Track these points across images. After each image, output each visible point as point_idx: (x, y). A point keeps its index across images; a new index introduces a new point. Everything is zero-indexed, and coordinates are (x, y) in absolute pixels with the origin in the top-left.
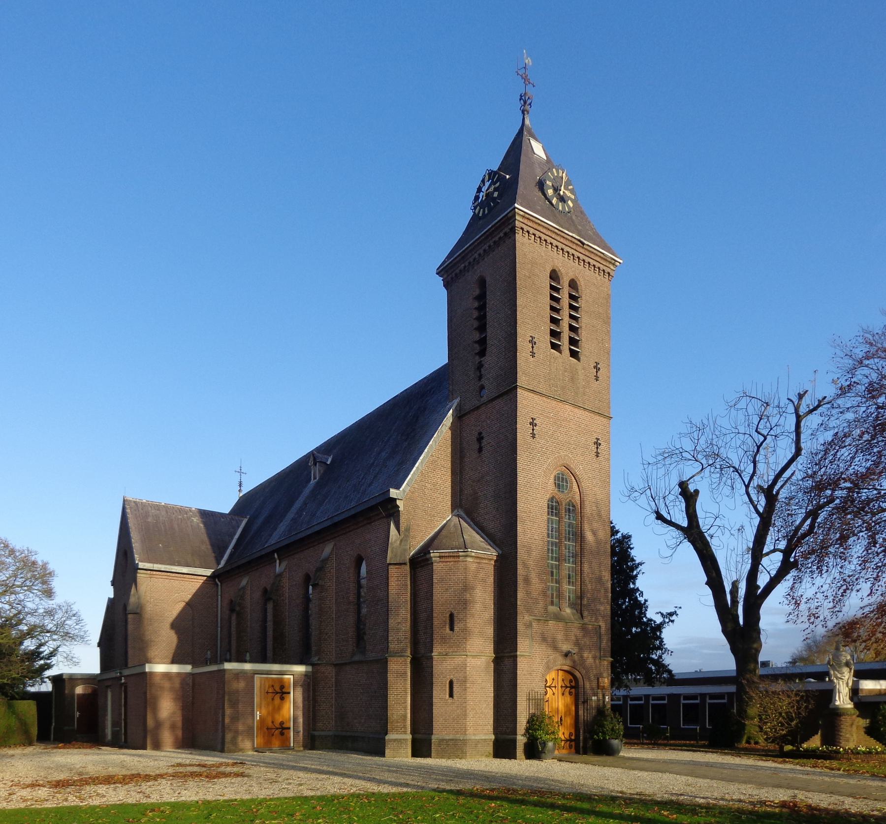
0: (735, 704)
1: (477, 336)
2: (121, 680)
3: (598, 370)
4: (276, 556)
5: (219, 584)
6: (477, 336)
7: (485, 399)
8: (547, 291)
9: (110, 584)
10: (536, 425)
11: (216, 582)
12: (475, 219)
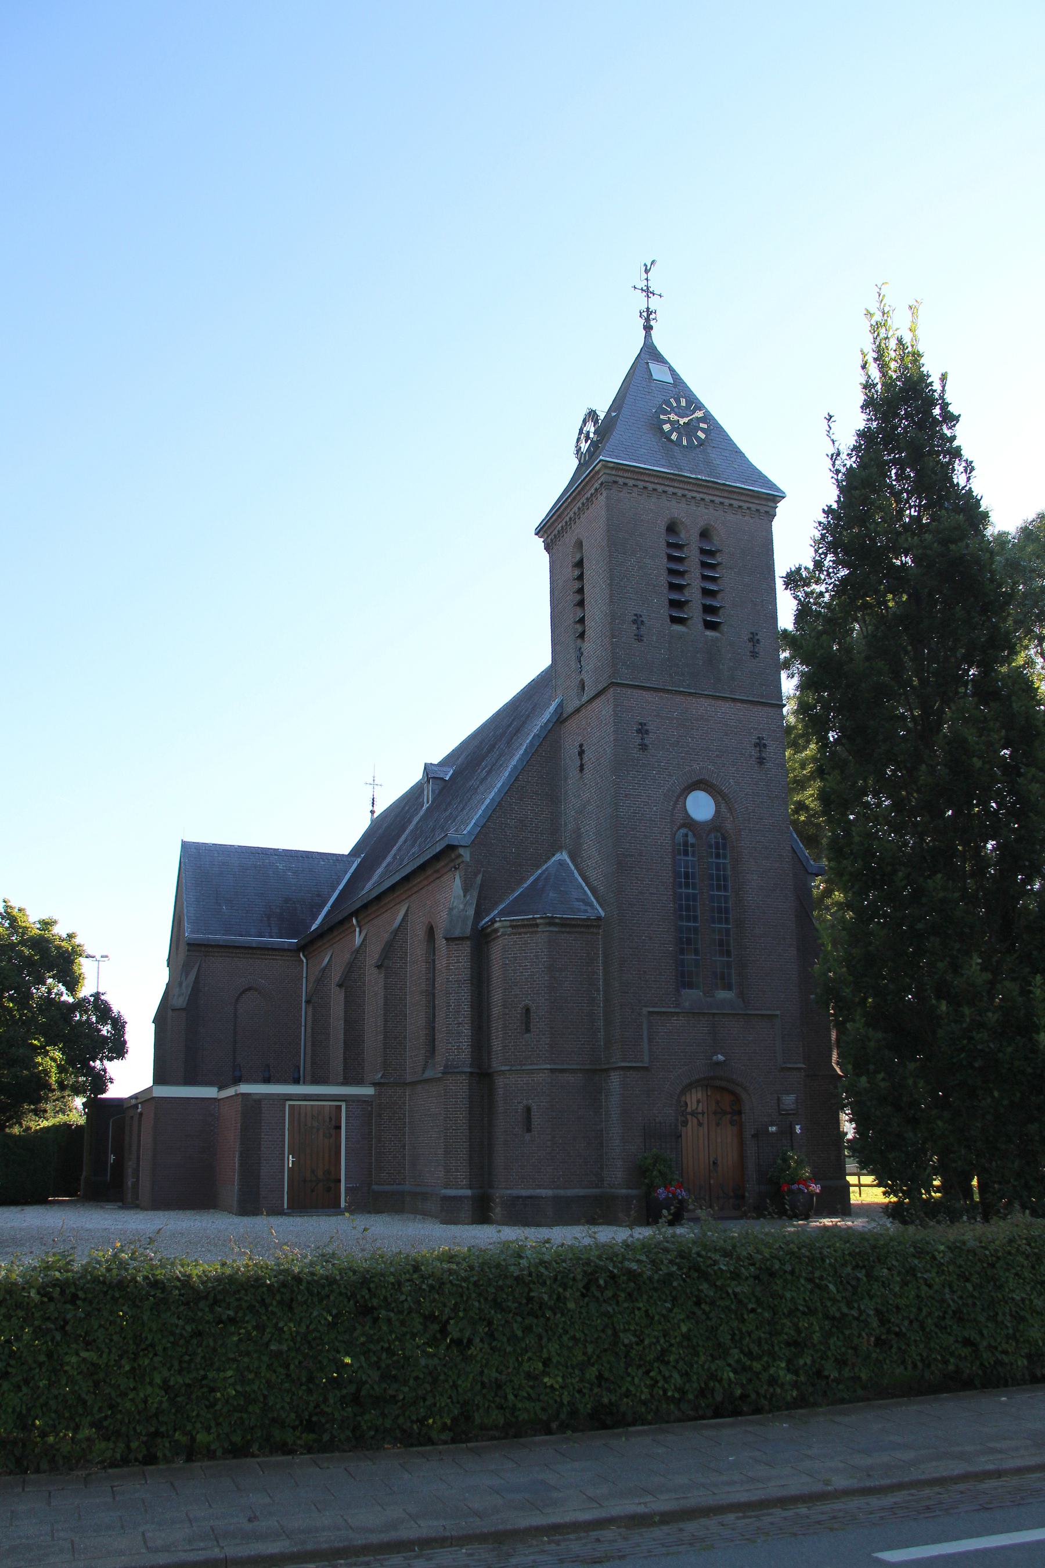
7: (585, 699)
9: (166, 963)
10: (647, 732)
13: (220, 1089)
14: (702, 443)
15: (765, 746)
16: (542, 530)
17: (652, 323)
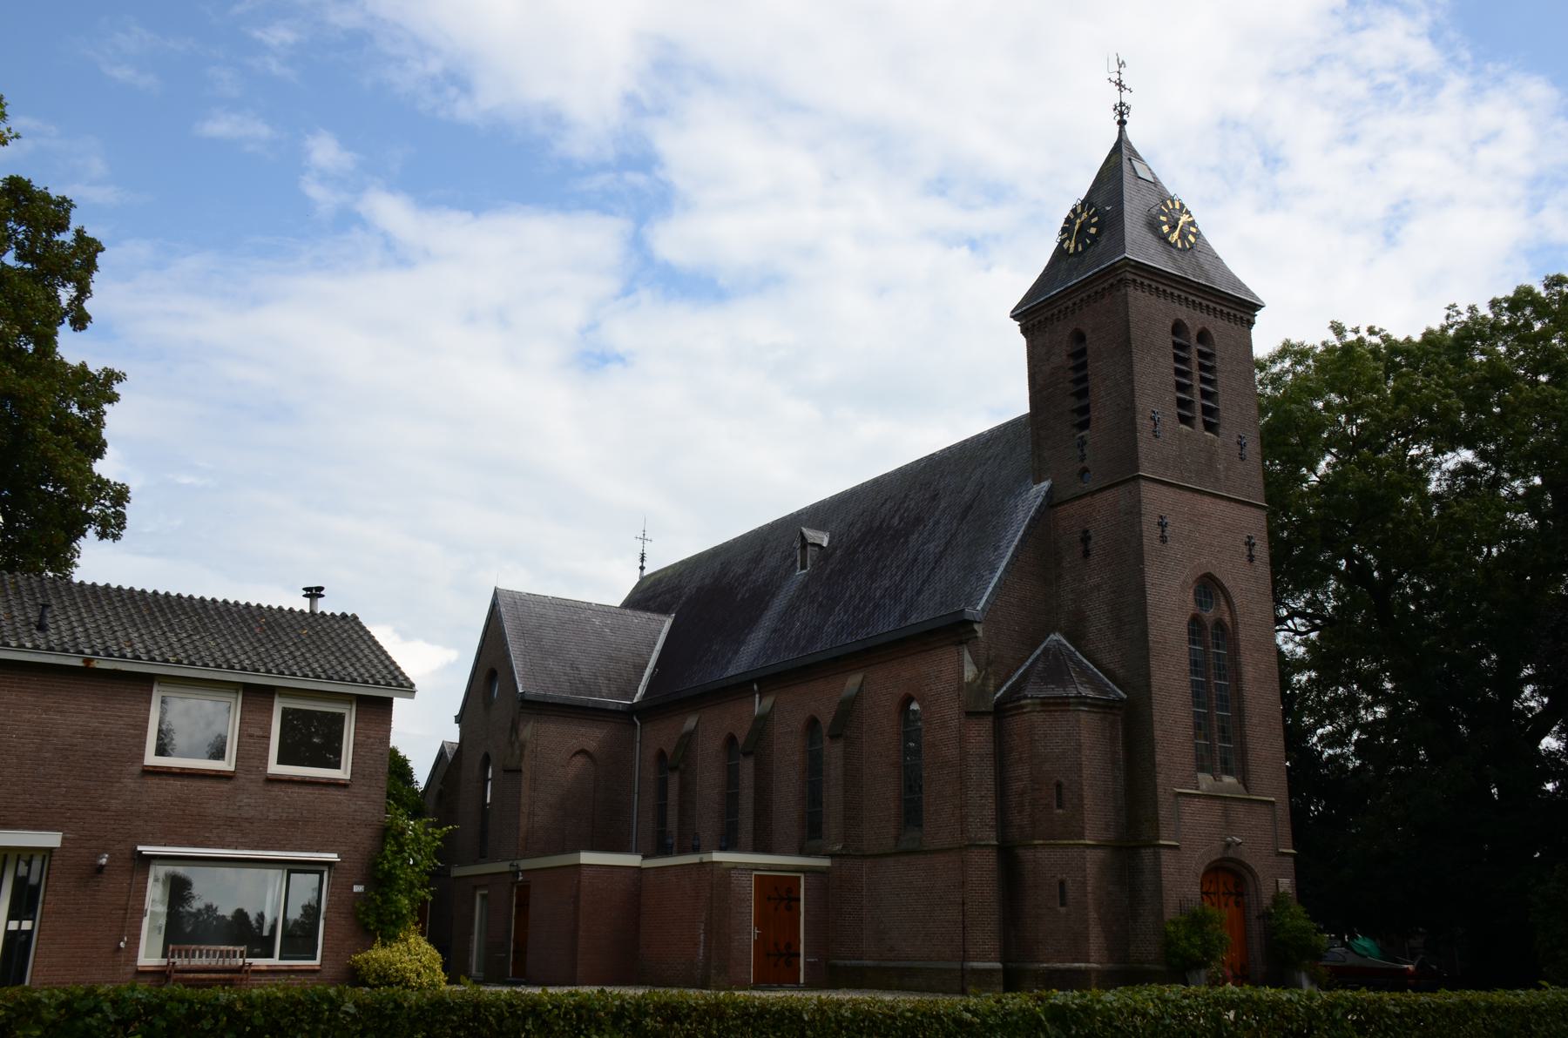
0: (717, 857)
1: (1074, 403)
2: (518, 876)
3: (1242, 446)
4: (755, 687)
5: (639, 724)
6: (1074, 403)
8: (1170, 350)
11: (633, 720)
12: (1060, 254)
13: (645, 857)
14: (1192, 246)
15: (1254, 544)
16: (1016, 315)
17: (1125, 117)
